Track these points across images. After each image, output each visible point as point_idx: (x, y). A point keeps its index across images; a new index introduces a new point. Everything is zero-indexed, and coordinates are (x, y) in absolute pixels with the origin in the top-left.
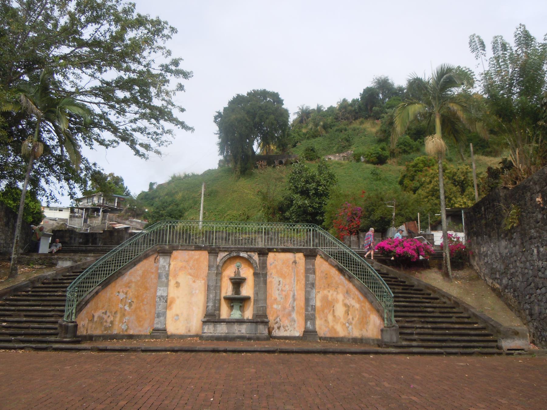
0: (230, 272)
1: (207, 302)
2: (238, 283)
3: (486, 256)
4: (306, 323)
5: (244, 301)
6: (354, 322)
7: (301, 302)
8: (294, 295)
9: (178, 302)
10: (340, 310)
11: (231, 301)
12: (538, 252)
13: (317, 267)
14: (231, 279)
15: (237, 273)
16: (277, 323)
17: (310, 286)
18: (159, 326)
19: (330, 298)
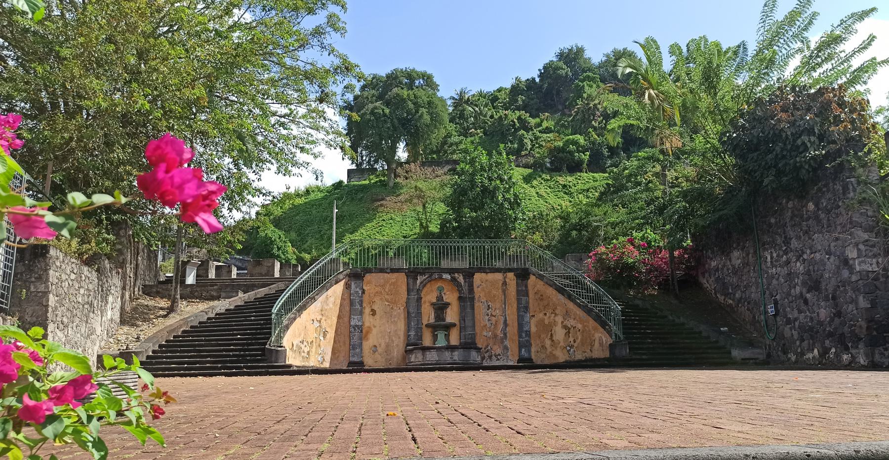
0: (430, 296)
1: (409, 331)
2: (440, 308)
3: (717, 270)
4: (520, 351)
5: (448, 327)
6: (576, 345)
7: (512, 330)
8: (506, 320)
9: (375, 331)
10: (559, 333)
11: (434, 328)
12: (772, 258)
13: (530, 288)
14: (433, 304)
15: (440, 298)
16: (488, 351)
17: (522, 308)
18: (355, 359)
19: (546, 322)
